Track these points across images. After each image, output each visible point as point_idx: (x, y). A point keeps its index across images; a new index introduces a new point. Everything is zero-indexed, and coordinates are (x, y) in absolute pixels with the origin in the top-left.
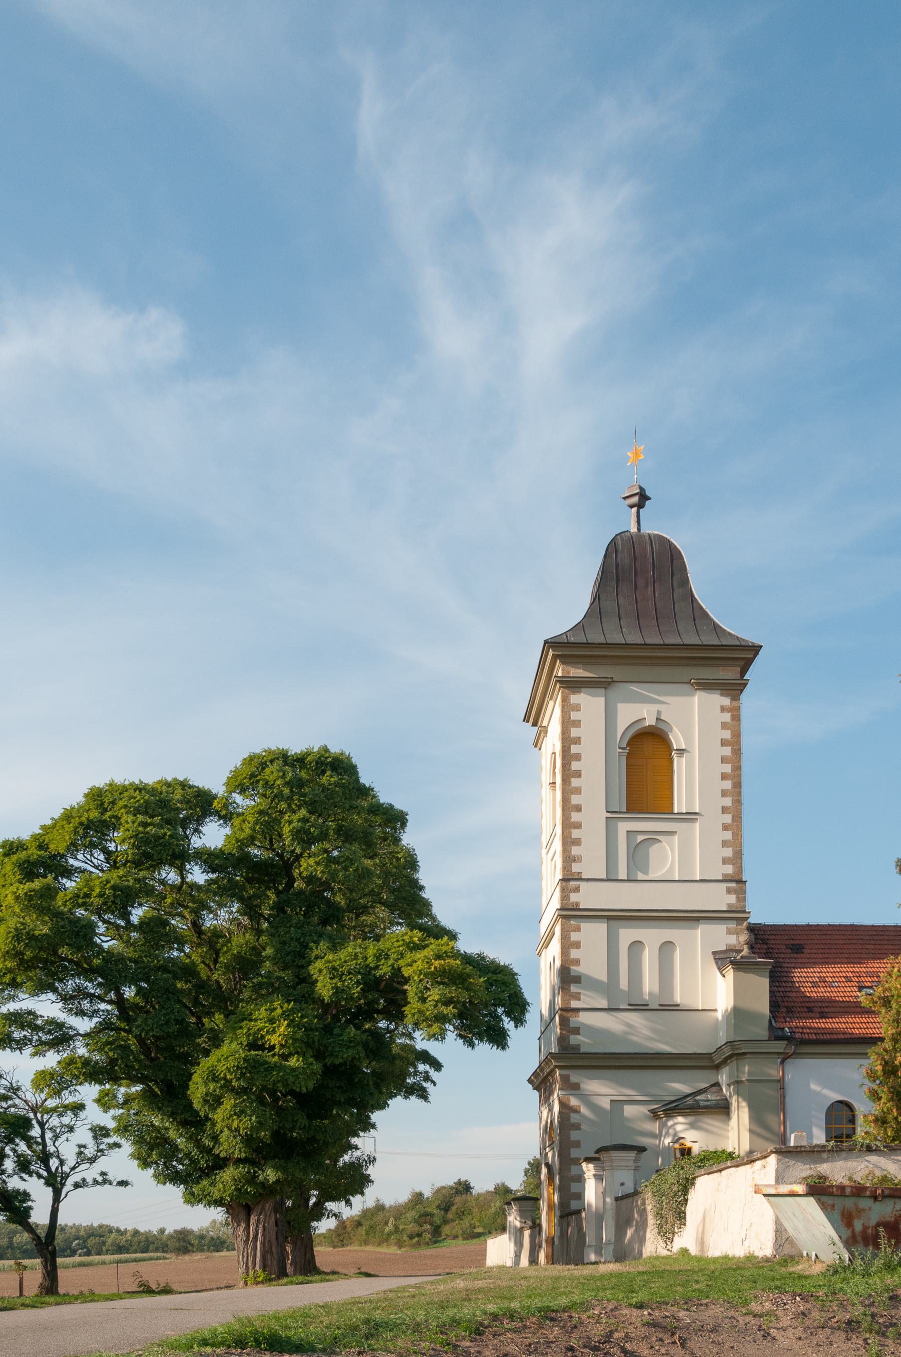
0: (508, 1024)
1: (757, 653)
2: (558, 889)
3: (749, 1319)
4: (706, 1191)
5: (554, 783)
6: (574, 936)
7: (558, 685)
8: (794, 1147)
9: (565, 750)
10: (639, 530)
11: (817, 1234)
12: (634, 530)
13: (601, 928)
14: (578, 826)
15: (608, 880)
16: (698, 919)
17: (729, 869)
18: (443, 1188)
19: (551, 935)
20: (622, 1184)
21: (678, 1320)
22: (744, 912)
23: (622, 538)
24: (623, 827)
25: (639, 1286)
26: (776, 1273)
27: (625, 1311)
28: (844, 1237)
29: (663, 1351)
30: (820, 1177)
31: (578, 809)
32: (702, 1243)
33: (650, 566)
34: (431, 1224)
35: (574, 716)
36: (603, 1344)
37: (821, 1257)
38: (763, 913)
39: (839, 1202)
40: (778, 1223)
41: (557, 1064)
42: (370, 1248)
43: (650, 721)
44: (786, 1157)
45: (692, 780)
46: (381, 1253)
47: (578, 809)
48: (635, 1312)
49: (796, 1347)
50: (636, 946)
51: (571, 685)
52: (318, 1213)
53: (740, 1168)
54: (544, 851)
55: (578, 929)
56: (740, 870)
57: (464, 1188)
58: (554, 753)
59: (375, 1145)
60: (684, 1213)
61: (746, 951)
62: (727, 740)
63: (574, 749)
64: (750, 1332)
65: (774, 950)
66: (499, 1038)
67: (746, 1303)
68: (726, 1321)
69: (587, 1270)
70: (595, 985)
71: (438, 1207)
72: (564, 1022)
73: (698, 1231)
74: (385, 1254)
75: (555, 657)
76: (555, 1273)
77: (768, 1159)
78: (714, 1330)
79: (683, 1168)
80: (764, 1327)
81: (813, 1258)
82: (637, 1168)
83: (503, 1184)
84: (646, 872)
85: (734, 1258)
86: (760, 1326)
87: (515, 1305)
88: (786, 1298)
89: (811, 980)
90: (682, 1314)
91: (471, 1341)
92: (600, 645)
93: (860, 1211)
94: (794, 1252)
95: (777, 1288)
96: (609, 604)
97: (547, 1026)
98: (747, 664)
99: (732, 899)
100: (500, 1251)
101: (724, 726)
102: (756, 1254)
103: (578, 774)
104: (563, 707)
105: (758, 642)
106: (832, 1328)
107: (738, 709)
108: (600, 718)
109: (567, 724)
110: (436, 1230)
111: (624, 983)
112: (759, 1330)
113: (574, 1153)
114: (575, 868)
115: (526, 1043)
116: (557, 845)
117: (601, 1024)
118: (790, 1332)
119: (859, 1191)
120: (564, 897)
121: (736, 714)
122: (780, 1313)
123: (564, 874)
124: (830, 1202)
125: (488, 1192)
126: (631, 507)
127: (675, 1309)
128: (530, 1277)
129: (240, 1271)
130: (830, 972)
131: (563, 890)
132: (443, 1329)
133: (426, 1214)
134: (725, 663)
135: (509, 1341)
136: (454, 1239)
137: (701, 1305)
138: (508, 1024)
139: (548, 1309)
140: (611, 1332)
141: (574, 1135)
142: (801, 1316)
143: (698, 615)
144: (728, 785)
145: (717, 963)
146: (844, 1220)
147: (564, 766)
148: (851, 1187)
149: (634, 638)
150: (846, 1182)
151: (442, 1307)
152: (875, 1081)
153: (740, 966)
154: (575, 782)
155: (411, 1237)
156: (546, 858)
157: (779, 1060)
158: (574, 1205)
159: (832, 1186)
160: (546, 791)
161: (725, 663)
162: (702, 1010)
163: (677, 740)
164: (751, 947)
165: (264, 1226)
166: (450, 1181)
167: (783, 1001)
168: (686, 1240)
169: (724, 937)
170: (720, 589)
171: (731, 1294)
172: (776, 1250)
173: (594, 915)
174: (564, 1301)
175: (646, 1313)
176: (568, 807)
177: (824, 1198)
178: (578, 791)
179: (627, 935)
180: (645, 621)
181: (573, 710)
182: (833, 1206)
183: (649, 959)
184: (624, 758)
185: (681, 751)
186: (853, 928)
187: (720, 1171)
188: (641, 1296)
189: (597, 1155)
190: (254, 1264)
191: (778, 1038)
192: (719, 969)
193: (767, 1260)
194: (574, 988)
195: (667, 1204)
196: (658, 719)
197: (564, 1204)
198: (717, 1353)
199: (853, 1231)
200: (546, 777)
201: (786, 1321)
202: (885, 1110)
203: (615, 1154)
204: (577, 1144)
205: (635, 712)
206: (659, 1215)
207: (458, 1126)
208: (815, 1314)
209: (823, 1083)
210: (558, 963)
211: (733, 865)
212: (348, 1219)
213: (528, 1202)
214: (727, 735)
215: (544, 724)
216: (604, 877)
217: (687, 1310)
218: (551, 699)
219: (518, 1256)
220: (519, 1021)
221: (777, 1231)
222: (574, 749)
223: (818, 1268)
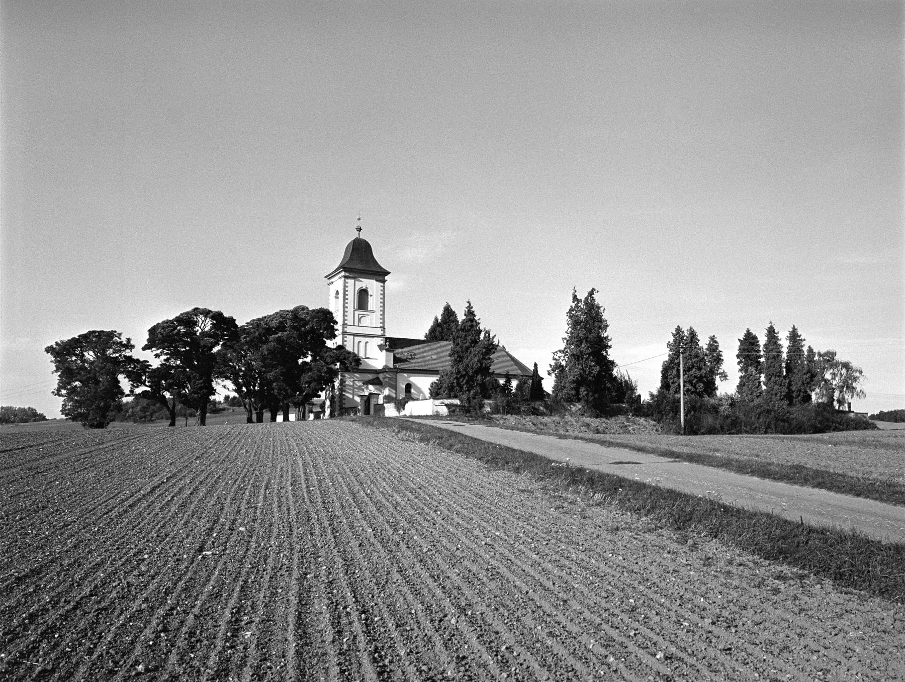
24: (357, 313)
38: (388, 335)
45: (373, 302)
65: (392, 344)
89: (403, 352)
108: (355, 285)
134: (380, 274)
146: (449, 409)
153: (387, 350)
155: (141, 418)
161: (380, 274)
169: (380, 341)
170: (381, 256)
173: (350, 334)
179: (357, 339)
180: (361, 261)
183: (362, 345)
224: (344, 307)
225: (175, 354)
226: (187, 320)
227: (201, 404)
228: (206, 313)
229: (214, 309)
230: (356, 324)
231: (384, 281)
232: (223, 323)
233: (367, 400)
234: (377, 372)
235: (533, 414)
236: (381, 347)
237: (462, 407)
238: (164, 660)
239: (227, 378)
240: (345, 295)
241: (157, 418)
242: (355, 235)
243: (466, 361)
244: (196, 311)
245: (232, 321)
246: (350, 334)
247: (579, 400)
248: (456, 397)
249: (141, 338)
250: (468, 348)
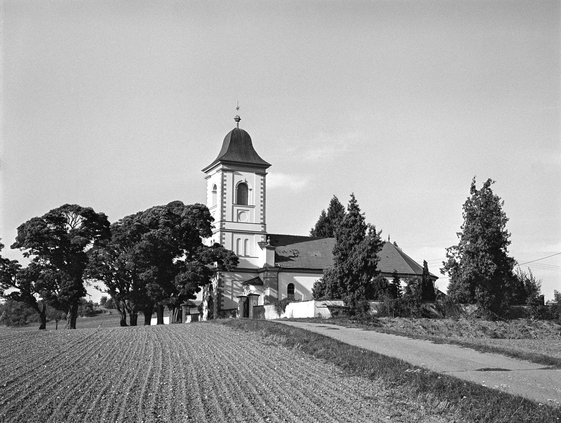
16: (254, 234)
17: (262, 221)
24: (236, 208)
38: (269, 232)
43: (243, 181)
45: (253, 197)
50: (239, 239)
55: (224, 234)
56: (265, 221)
65: (274, 241)
89: (285, 250)
99: (263, 229)
114: (224, 218)
120: (221, 226)
121: (264, 180)
134: (261, 167)
153: (268, 248)
161: (261, 167)
170: (260, 148)
173: (229, 231)
179: (236, 236)
180: (240, 153)
183: (241, 243)
185: (251, 190)
186: (289, 236)
224: (223, 202)
225: (44, 253)
226: (57, 217)
227: (72, 305)
228: (77, 210)
229: (84, 205)
230: (235, 220)
231: (264, 175)
232: (95, 221)
233: (246, 301)
234: (257, 271)
235: (424, 316)
236: (261, 245)
237: (346, 309)
239: (100, 278)
240: (223, 189)
241: (31, 321)
242: (234, 125)
243: (350, 259)
244: (66, 207)
245: (103, 219)
246: (229, 231)
247: (474, 302)
248: (339, 298)
249: (13, 236)
250: (351, 245)
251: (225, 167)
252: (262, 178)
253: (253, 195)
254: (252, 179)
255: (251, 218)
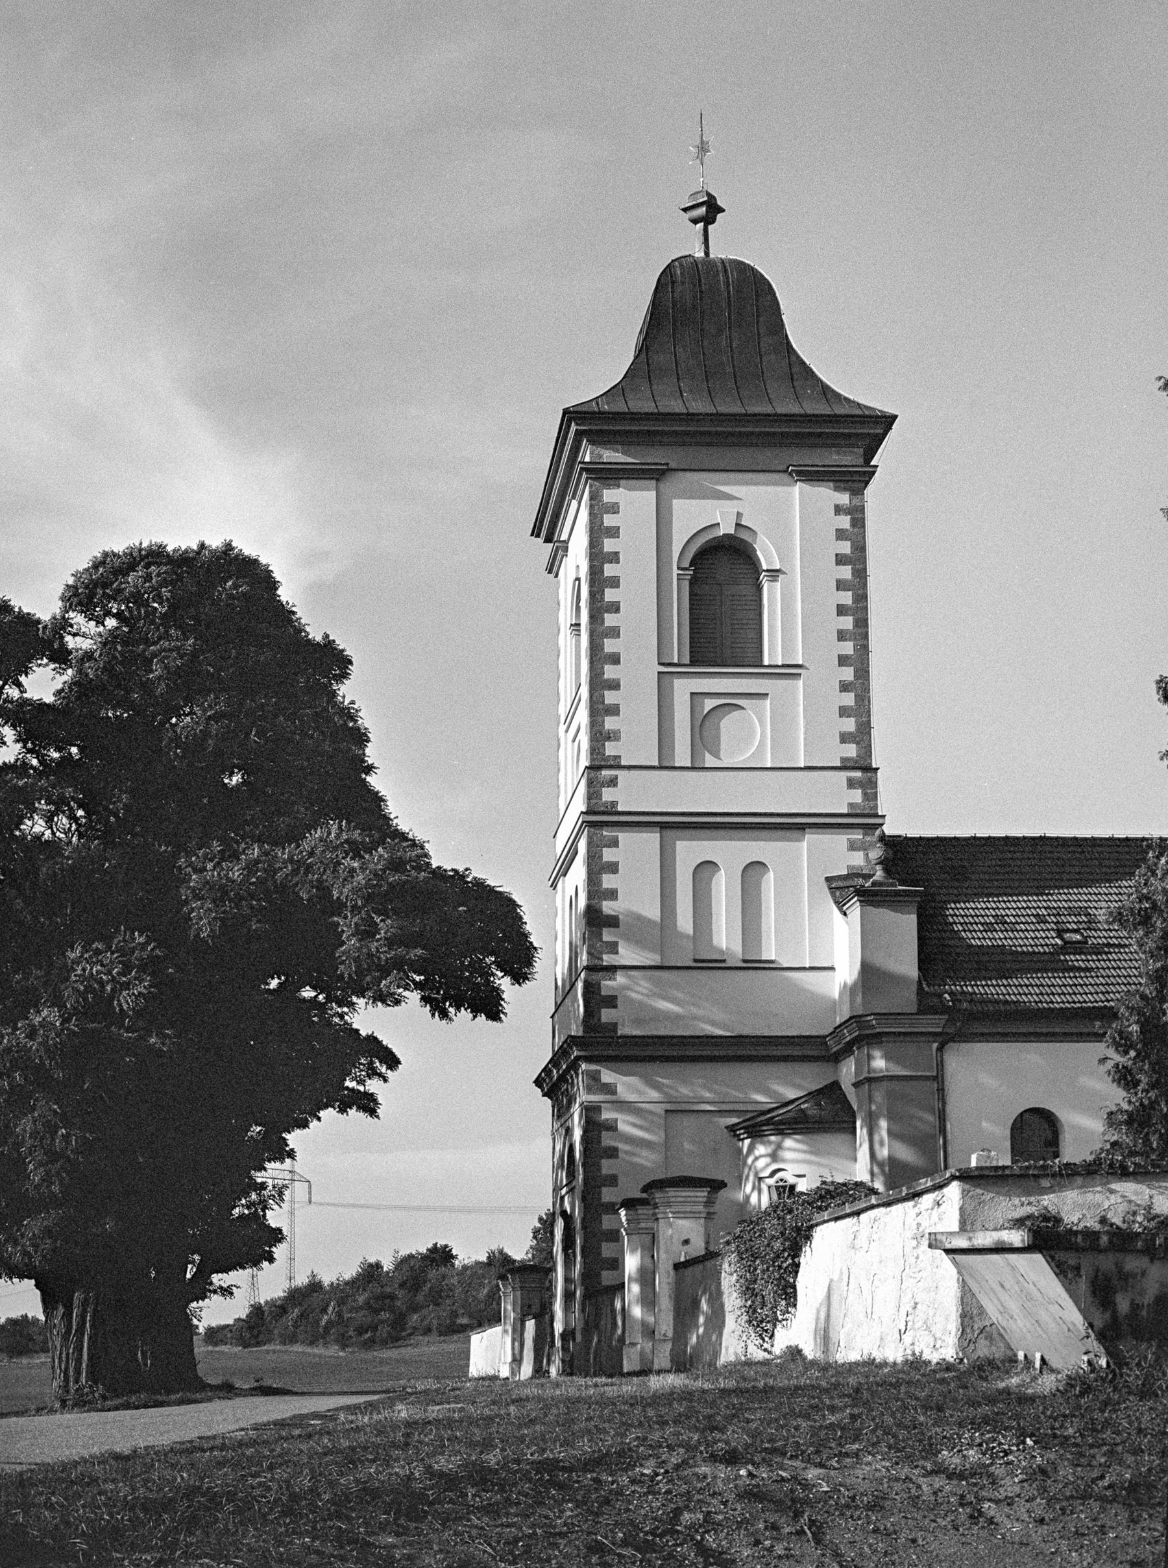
0: (504, 983)
1: (889, 427)
2: (583, 782)
3: (939, 1481)
4: (829, 1249)
5: (578, 625)
6: (608, 855)
7: (584, 475)
8: (977, 1168)
9: (595, 572)
10: (707, 254)
11: (1046, 1321)
12: (700, 254)
13: (652, 839)
14: (615, 685)
15: (661, 768)
16: (802, 828)
17: (851, 751)
18: (411, 1256)
19: (572, 853)
20: (686, 1242)
21: (806, 1486)
22: (876, 816)
23: (681, 265)
24: (683, 688)
25: (726, 1417)
26: (964, 1394)
27: (704, 1469)
28: (1098, 1324)
29: (779, 1550)
30: (1046, 1218)
31: (615, 659)
32: (825, 1337)
33: (724, 305)
34: (392, 1311)
35: (609, 520)
36: (661, 1536)
37: (1054, 1362)
38: (903, 819)
39: (1088, 1263)
40: (967, 1298)
41: (582, 1053)
42: (298, 1348)
43: (727, 528)
44: (978, 1186)
45: (791, 616)
46: (315, 1356)
47: (615, 659)
48: (722, 1471)
49: (1036, 1539)
50: (706, 868)
51: (606, 475)
52: (201, 1289)
53: (894, 1208)
54: (562, 728)
55: (615, 843)
56: (866, 750)
57: (441, 1256)
58: (578, 579)
59: (310, 1193)
60: (794, 1287)
61: (879, 874)
62: (845, 555)
63: (609, 570)
64: (945, 1507)
65: (918, 876)
66: (489, 1006)
67: (931, 1451)
68: (897, 1486)
69: (629, 1388)
70: (639, 932)
71: (402, 1285)
72: (591, 990)
73: (818, 1319)
74: (320, 1356)
75: (579, 434)
76: (572, 1392)
77: (945, 1190)
78: (875, 1506)
79: (790, 1211)
80: (970, 1498)
81: (1038, 1364)
82: (709, 1216)
83: (501, 1252)
84: (717, 755)
85: (885, 1364)
86: (962, 1497)
87: (493, 1458)
88: (1006, 1440)
89: (975, 918)
90: (812, 1474)
91: (398, 1535)
92: (648, 416)
93: (1125, 1277)
94: (998, 1352)
95: (986, 1420)
96: (661, 359)
97: (564, 995)
98: (873, 445)
99: (857, 796)
100: (490, 1352)
101: (841, 534)
102: (926, 1356)
103: (615, 608)
104: (591, 506)
105: (890, 410)
106: (1101, 1498)
107: (862, 509)
108: (650, 524)
109: (597, 533)
110: (399, 1322)
111: (685, 922)
112: (962, 1505)
113: (608, 1195)
114: (610, 749)
115: (532, 1012)
116: (583, 716)
117: (648, 1002)
118: (1021, 1508)
119: (1121, 1239)
120: (593, 794)
121: (857, 515)
122: (998, 1471)
123: (592, 760)
124: (1072, 1262)
125: (478, 1263)
126: (695, 221)
127: (797, 1463)
128: (527, 1399)
129: (55, 1383)
130: (1012, 907)
131: (590, 783)
132: (341, 1505)
133: (383, 1297)
135: (474, 1532)
136: (425, 1334)
137: (847, 1455)
138: (504, 983)
139: (552, 1466)
140: (678, 1512)
141: (607, 1167)
142: (1039, 1476)
143: (800, 374)
144: (847, 622)
145: (833, 894)
147: (592, 595)
148: (1107, 1232)
149: (700, 406)
150: (1092, 1224)
151: (351, 1459)
152: (1126, 1053)
153: (870, 897)
154: (610, 620)
156: (565, 739)
157: (935, 1045)
158: (607, 1278)
159: (1070, 1232)
160: (565, 638)
161: (839, 442)
162: (812, 968)
163: (767, 555)
164: (887, 870)
165: (95, 1310)
166: (421, 1247)
167: (938, 951)
168: (797, 1332)
169: (842, 854)
170: (835, 344)
171: (902, 1434)
172: (963, 1350)
174: (585, 1447)
175: (743, 1472)
176: (598, 657)
177: (1061, 1255)
178: (615, 632)
179: (690, 852)
180: (714, 380)
181: (608, 512)
182: (1077, 1269)
184: (686, 585)
185: (774, 574)
187: (858, 1213)
188: (736, 1437)
189: (644, 1195)
190: (78, 1372)
191: (933, 1010)
192: (837, 903)
193: (948, 1367)
194: (607, 936)
195: (763, 1271)
196: (738, 525)
197: (590, 1276)
198: (886, 1554)
199: (1115, 1311)
200: (565, 617)
201: (1010, 1486)
202: (1146, 1102)
203: (672, 1192)
204: (613, 1180)
205: (700, 512)
206: (749, 1290)
207: (427, 1151)
208: (1066, 1472)
209: (989, 1085)
210: (582, 902)
211: (857, 743)
212: (267, 1302)
213: (530, 1277)
214: (845, 548)
215: (564, 537)
216: (656, 763)
217: (821, 1465)
218: (574, 497)
219: (517, 1360)
220: (520, 977)
221: (963, 1316)
222: (609, 570)
223: (1048, 1383)
230: (682, 757)
231: (855, 480)
238: (843, 1429)
251: (611, 456)
252: (844, 499)
253: (787, 608)
254: (783, 516)
255: (781, 737)
